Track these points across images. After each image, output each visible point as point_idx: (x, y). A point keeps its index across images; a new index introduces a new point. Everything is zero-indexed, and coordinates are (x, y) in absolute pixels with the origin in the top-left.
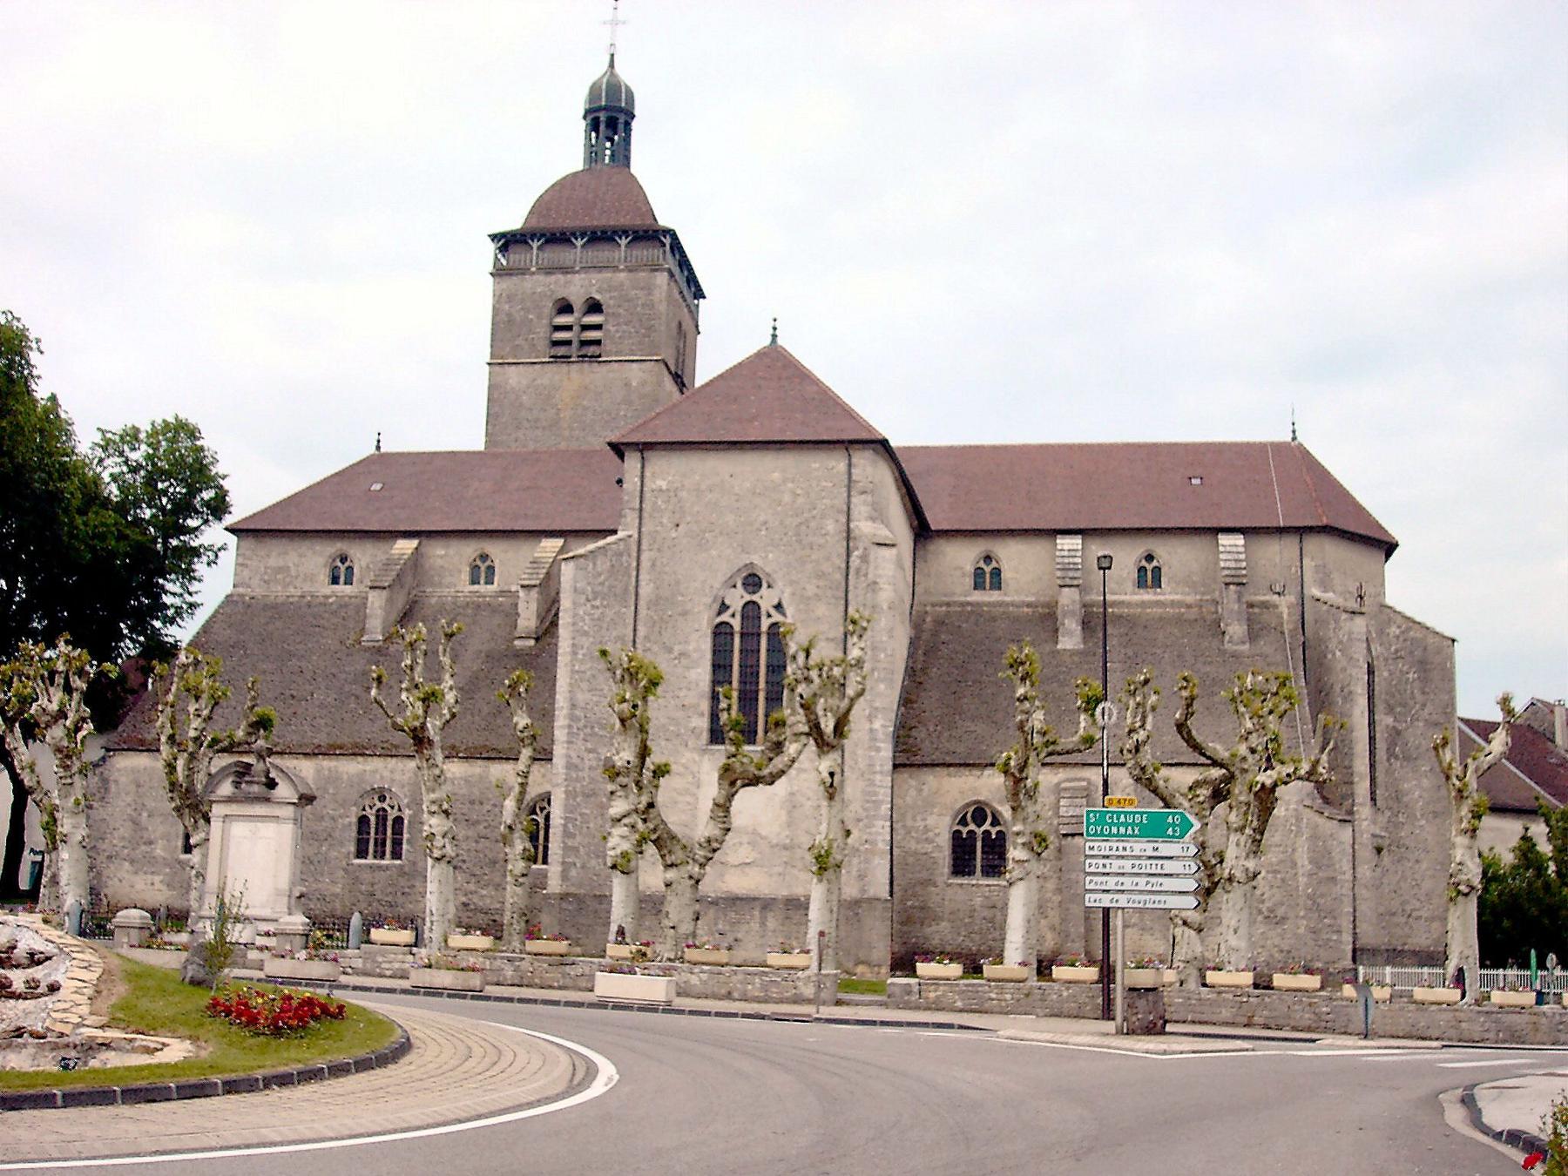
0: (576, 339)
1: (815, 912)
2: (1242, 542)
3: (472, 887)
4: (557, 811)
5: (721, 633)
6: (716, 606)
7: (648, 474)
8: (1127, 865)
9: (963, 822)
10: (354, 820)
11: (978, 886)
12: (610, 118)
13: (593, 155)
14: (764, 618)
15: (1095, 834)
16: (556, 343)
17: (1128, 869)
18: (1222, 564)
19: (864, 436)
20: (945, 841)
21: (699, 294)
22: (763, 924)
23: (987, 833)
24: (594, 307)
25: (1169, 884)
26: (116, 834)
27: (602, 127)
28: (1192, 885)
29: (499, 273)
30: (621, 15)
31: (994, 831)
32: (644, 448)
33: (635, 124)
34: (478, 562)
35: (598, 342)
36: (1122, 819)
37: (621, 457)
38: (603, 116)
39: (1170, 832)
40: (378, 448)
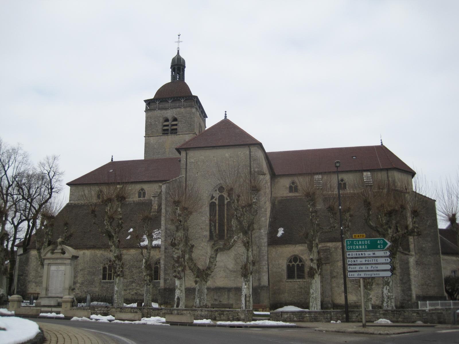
0: (169, 128)
1: (245, 291)
2: (370, 174)
3: (138, 288)
4: (162, 262)
5: (212, 205)
6: (210, 197)
7: (188, 157)
8: (363, 261)
9: (290, 262)
10: (102, 268)
11: (296, 281)
12: (178, 66)
13: (173, 77)
14: (225, 200)
15: (350, 249)
16: (164, 130)
17: (364, 262)
18: (365, 180)
19: (254, 142)
20: (285, 267)
21: (205, 116)
22: (228, 296)
23: (298, 265)
24: (175, 119)
25: (380, 267)
26: (31, 274)
27: (176, 70)
28: (389, 267)
29: (147, 111)
30: (180, 40)
31: (300, 264)
32: (186, 149)
33: (186, 69)
34: (141, 191)
35: (176, 129)
36: (360, 243)
37: (180, 153)
38: (176, 67)
39: (379, 247)
40: (112, 160)
